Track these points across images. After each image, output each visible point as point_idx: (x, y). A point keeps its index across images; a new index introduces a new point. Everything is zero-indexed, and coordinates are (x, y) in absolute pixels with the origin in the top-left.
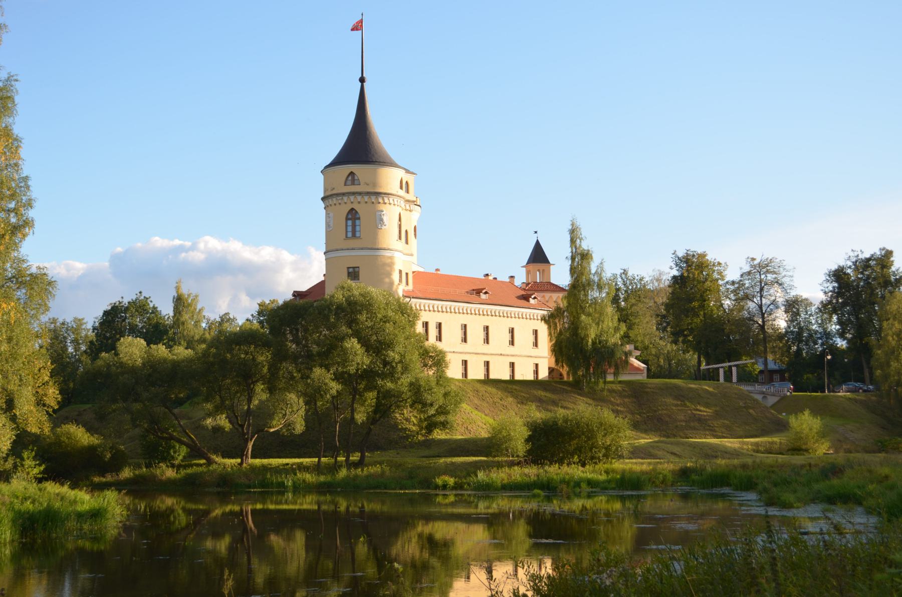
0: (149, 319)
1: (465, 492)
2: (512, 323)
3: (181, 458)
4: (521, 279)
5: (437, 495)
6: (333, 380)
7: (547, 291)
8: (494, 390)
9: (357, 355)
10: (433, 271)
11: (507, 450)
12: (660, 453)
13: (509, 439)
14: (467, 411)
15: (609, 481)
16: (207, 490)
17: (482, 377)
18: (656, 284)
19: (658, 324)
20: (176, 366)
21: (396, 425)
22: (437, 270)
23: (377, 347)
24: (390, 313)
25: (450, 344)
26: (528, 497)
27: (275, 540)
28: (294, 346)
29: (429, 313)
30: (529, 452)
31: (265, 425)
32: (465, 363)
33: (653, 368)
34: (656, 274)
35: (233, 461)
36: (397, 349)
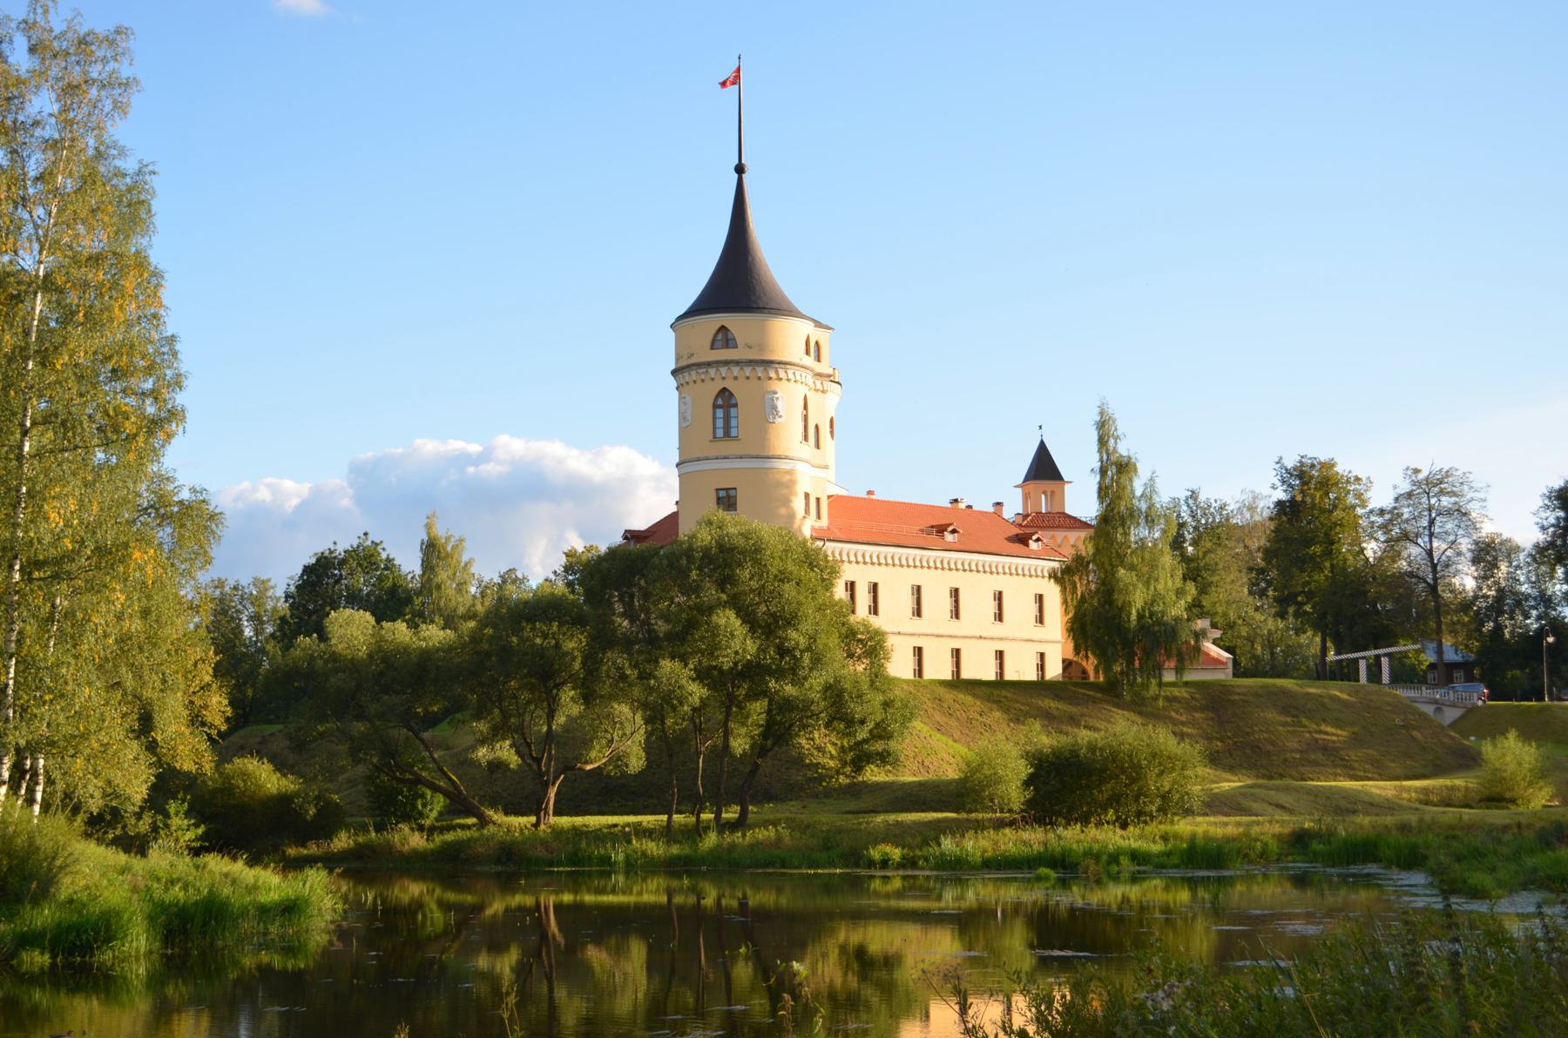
3: (434, 814)
4: (1014, 507)
5: (872, 877)
6: (694, 680)
8: (969, 699)
10: (863, 495)
11: (992, 800)
12: (1256, 806)
13: (996, 780)
14: (922, 735)
15: (1168, 854)
16: (478, 868)
17: (948, 676)
20: (426, 656)
22: (870, 493)
24: (791, 567)
25: (893, 618)
26: (1029, 880)
27: (596, 956)
29: (857, 567)
30: (1030, 804)
32: (919, 652)
34: (1247, 498)
36: (804, 627)
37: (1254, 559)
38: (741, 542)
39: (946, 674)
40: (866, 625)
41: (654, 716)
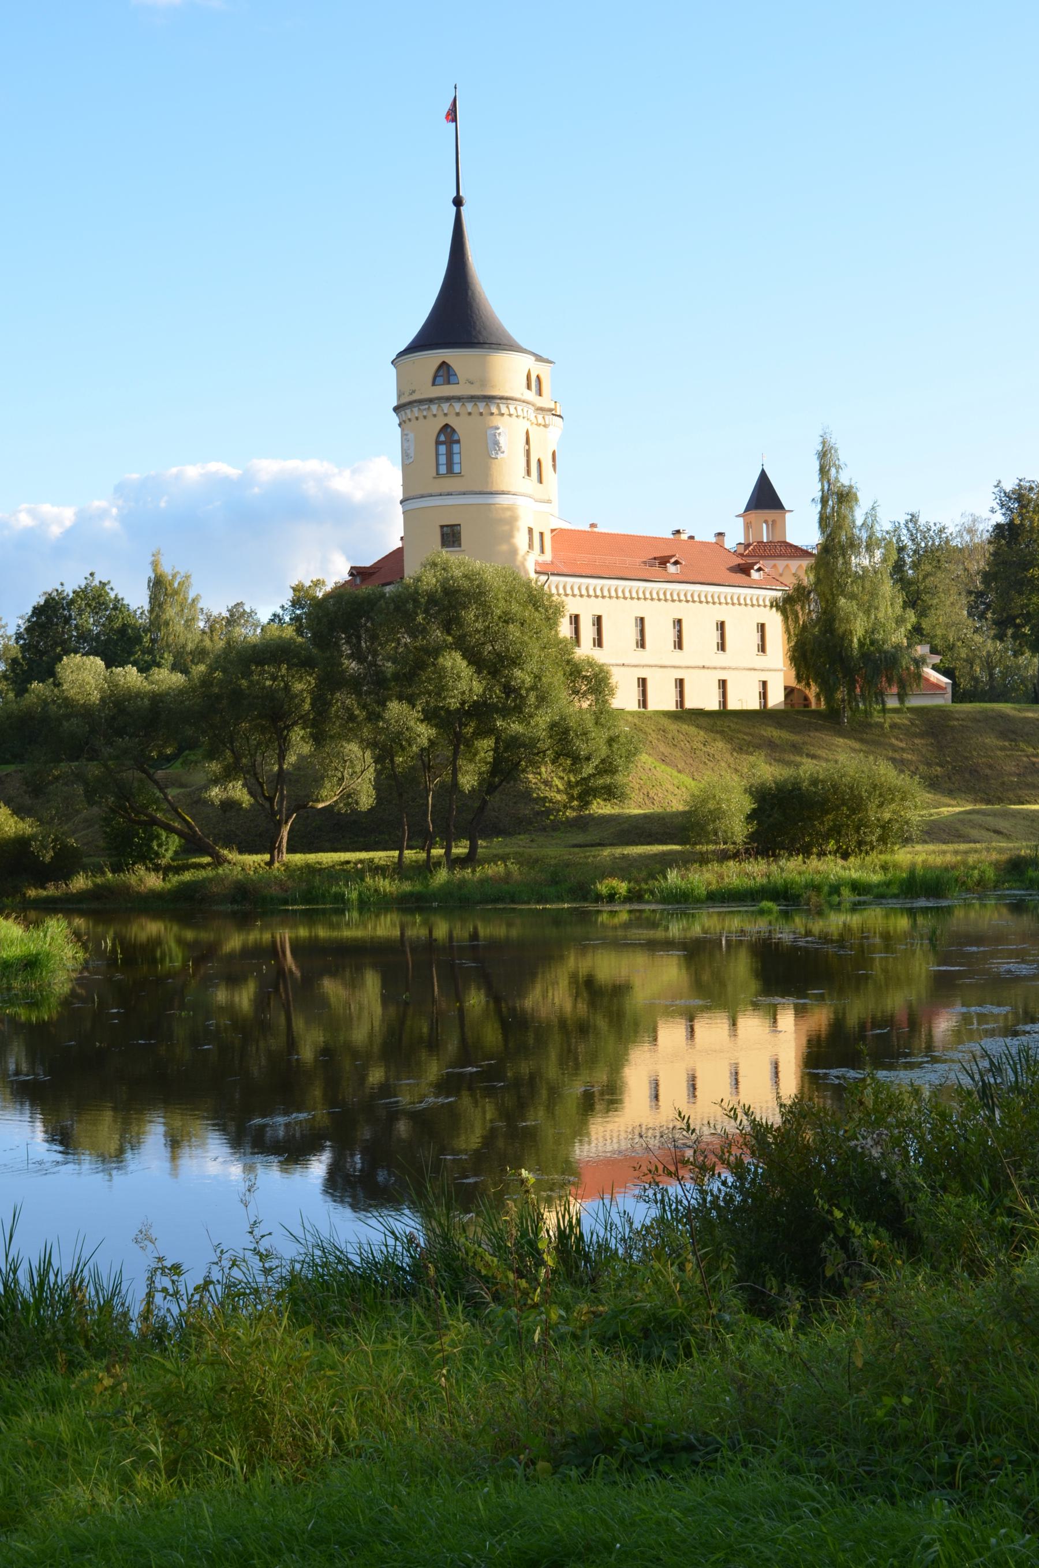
0: (109, 618)
1: (647, 907)
2: (721, 613)
3: (169, 854)
4: (735, 537)
5: (599, 912)
6: (422, 721)
7: (780, 556)
8: (692, 730)
9: (462, 680)
11: (716, 834)
12: (974, 833)
13: (717, 815)
14: (647, 767)
15: (888, 884)
16: (215, 908)
17: (672, 706)
18: (967, 538)
19: (970, 607)
20: (157, 699)
21: (528, 792)
22: (593, 525)
23: (493, 665)
24: (515, 608)
25: (616, 656)
26: (753, 912)
27: (331, 988)
28: (353, 665)
29: (578, 599)
30: (752, 837)
31: (309, 797)
32: (643, 682)
33: (964, 683)
34: (967, 521)
35: (257, 858)
36: (528, 667)
37: (973, 582)
38: (465, 584)
39: (669, 704)
40: (591, 664)
41: (384, 754)
